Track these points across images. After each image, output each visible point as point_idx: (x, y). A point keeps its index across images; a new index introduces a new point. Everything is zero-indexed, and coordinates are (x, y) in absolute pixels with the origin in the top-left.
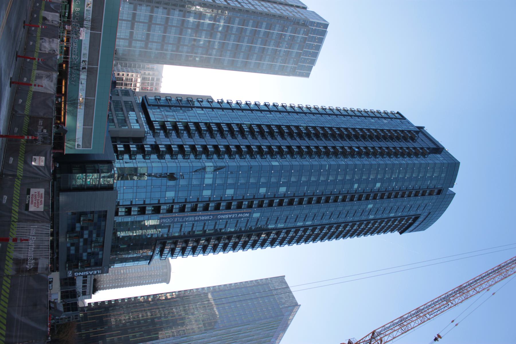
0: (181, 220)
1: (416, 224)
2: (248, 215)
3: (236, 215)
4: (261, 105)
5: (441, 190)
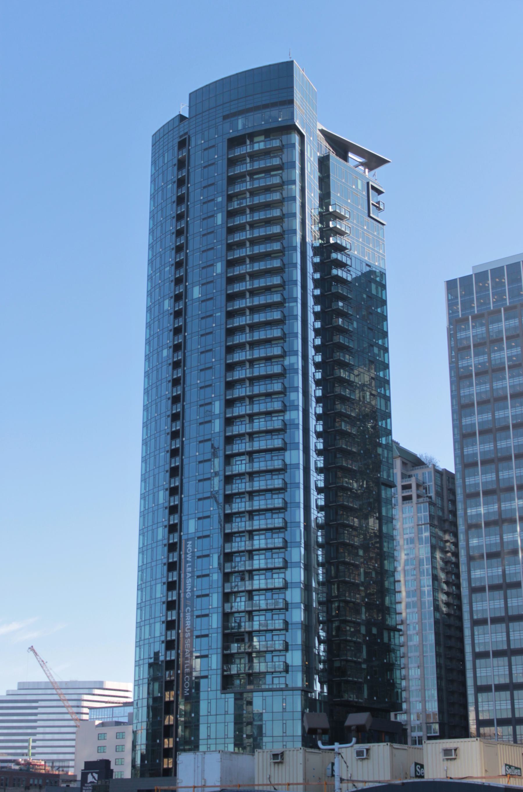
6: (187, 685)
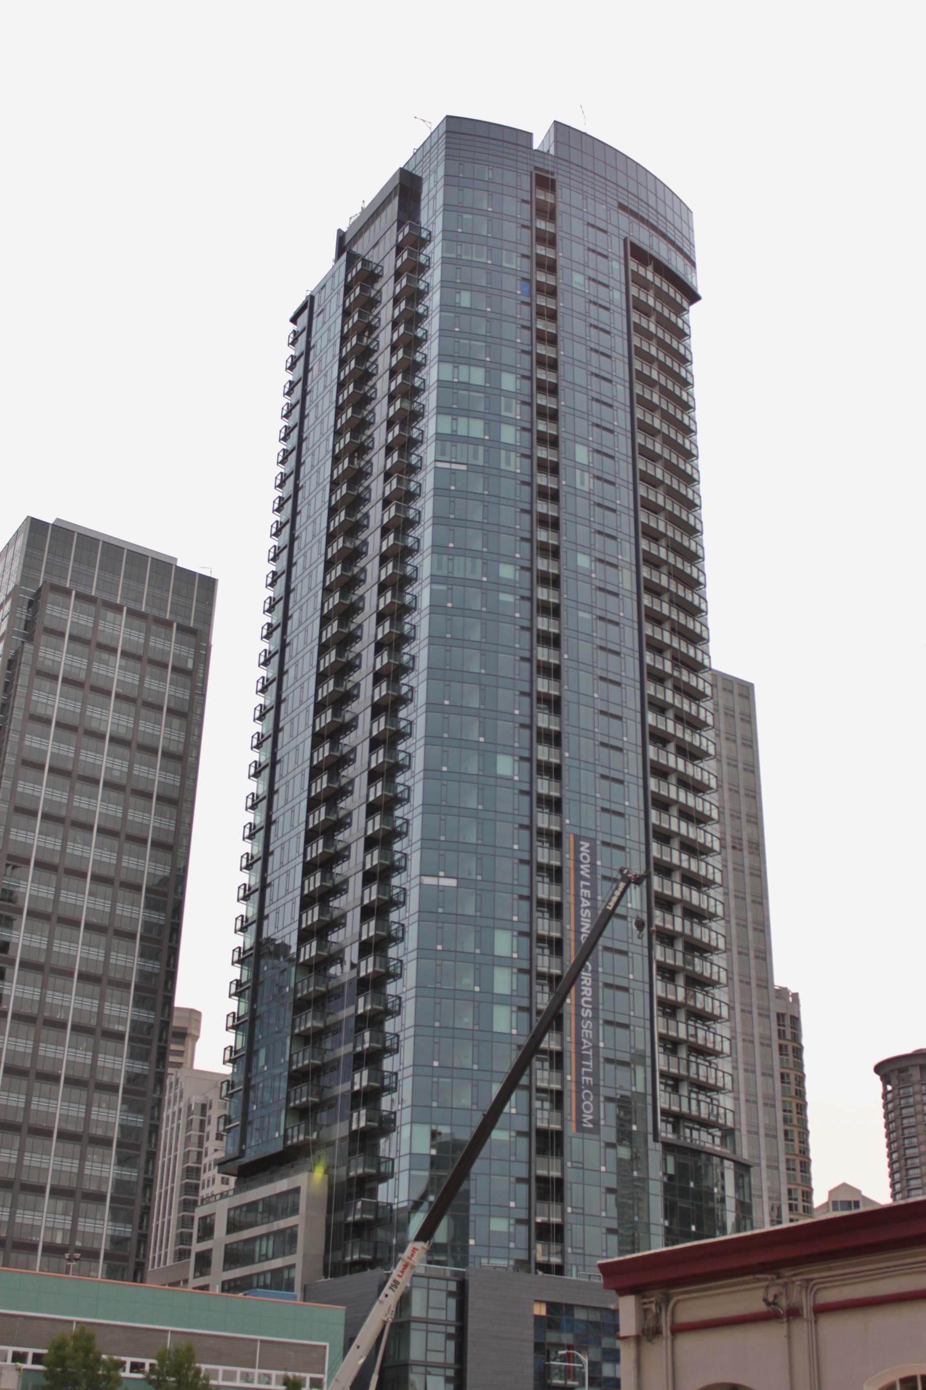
0: (591, 1063)
1: (662, 251)
2: (585, 846)
3: (582, 883)
4: (260, 731)
5: (537, 175)
6: (588, 1107)
